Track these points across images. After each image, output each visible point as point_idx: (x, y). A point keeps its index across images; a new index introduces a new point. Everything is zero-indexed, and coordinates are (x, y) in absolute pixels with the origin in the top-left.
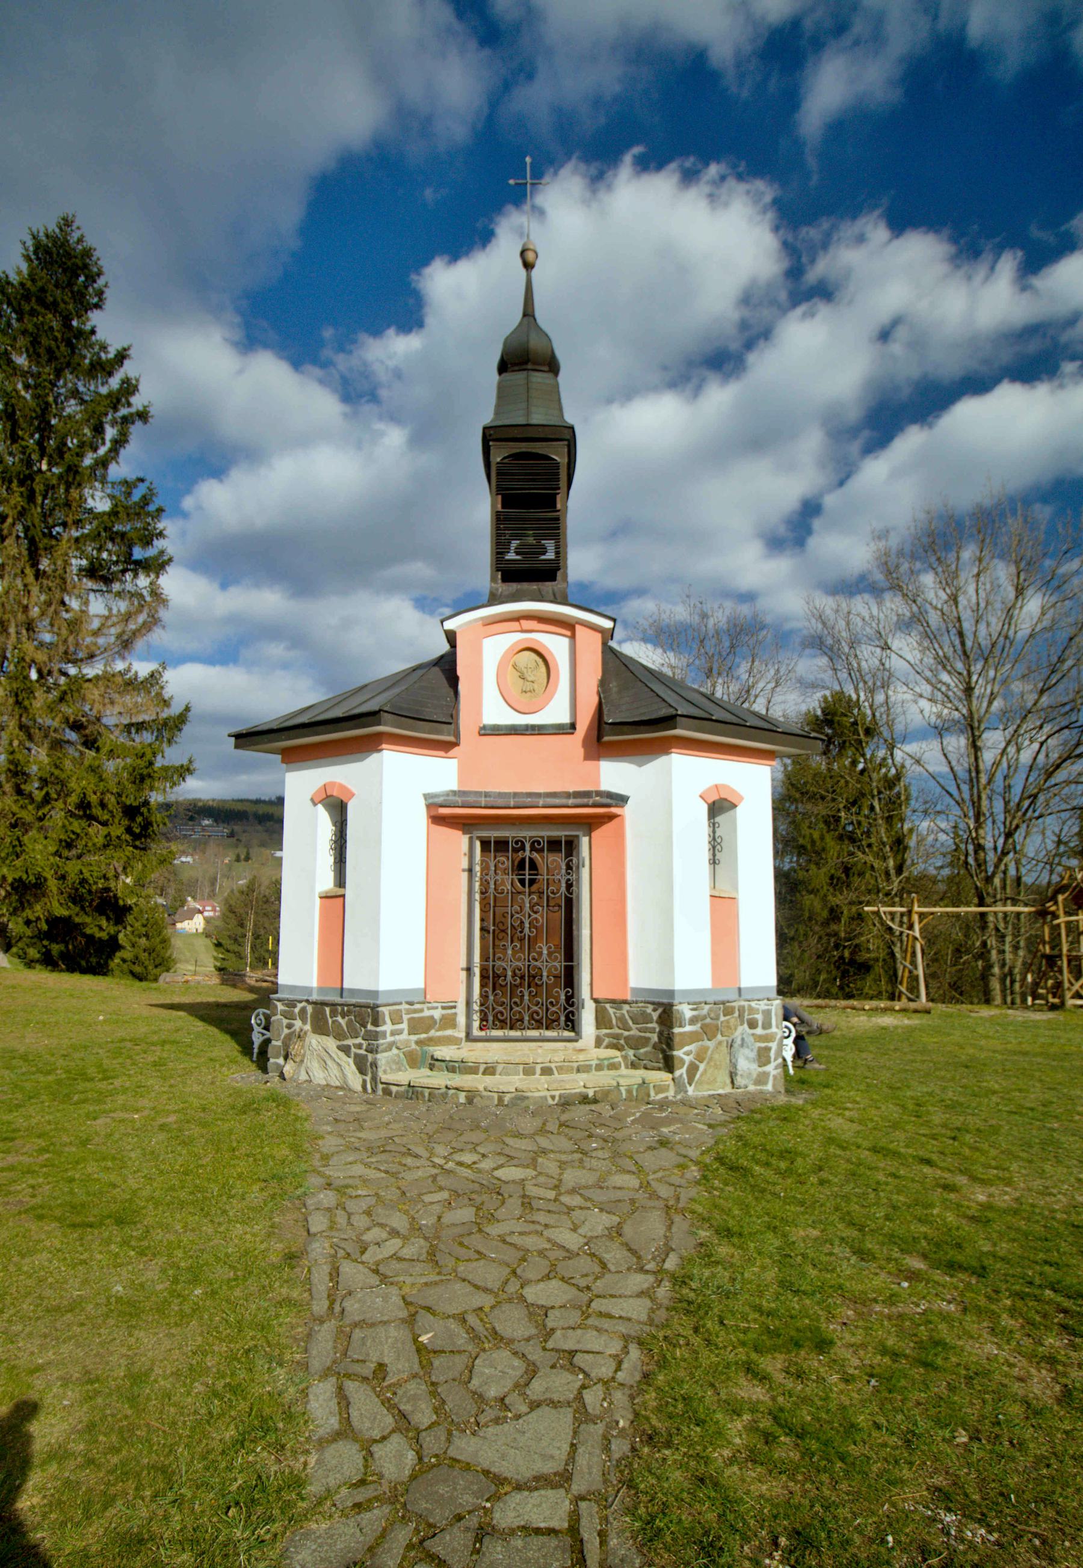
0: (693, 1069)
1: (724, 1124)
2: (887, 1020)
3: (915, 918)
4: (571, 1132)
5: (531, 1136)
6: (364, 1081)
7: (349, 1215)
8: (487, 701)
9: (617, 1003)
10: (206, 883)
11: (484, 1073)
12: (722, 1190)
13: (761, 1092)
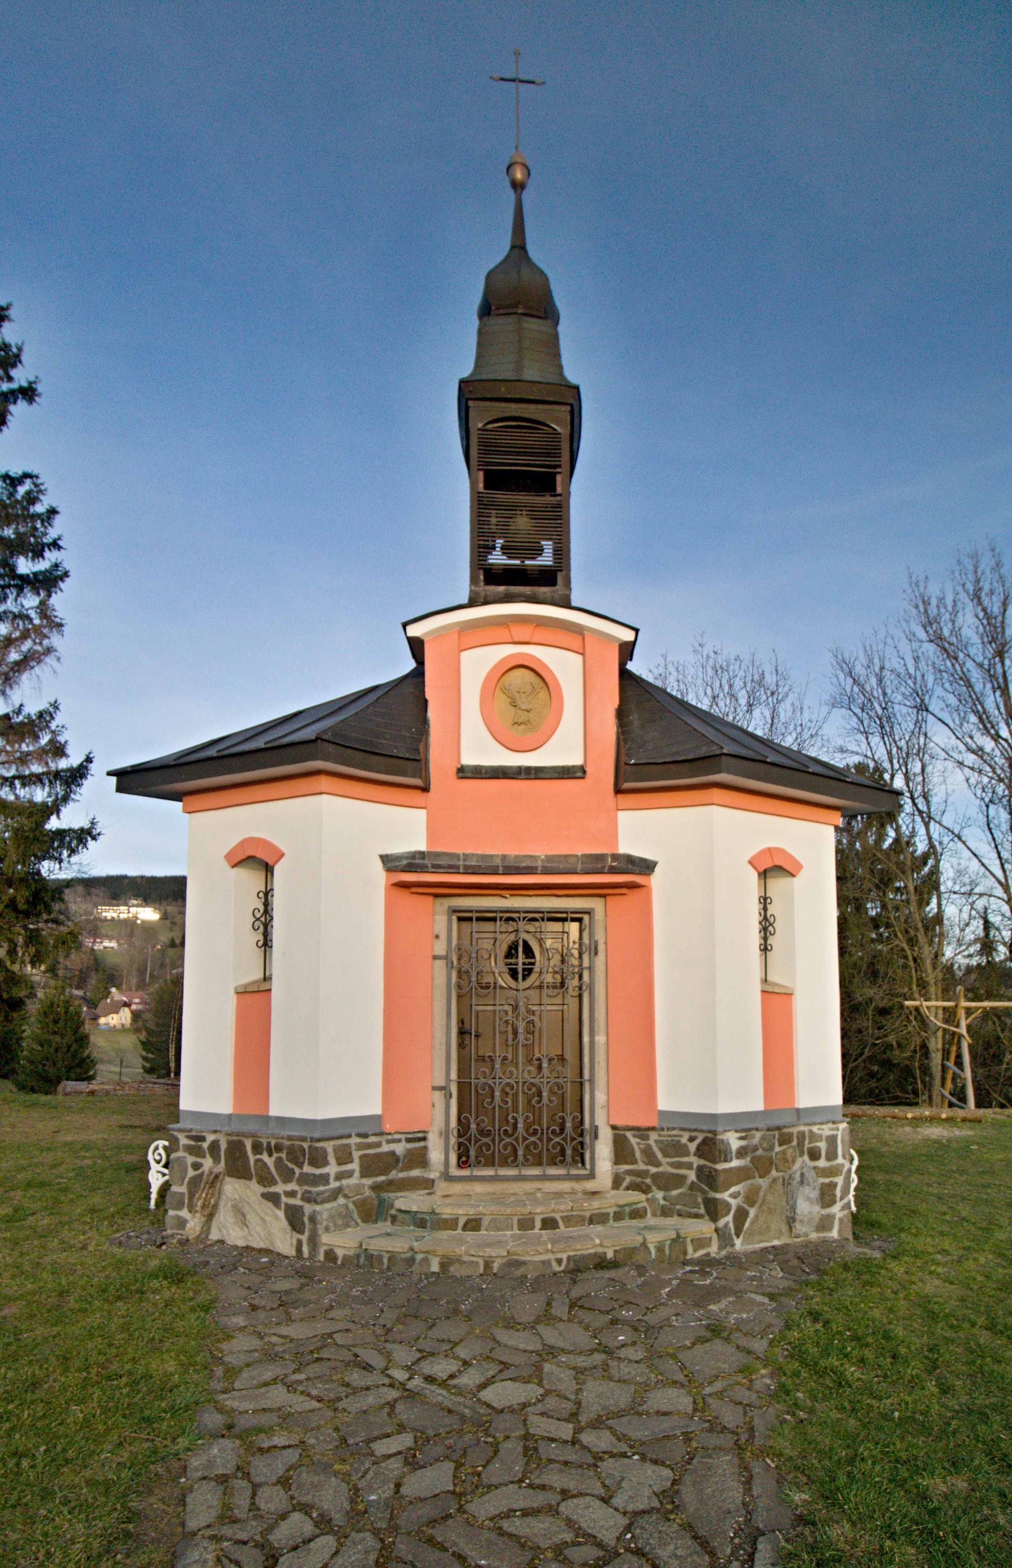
0: (741, 1215)
1: (788, 1292)
2: (935, 1132)
3: (962, 1014)
4: (587, 1317)
5: (532, 1326)
6: (300, 1243)
7: (255, 1487)
8: (468, 734)
9: (643, 1132)
10: (135, 973)
11: (465, 1228)
12: (812, 1411)
13: (825, 1241)
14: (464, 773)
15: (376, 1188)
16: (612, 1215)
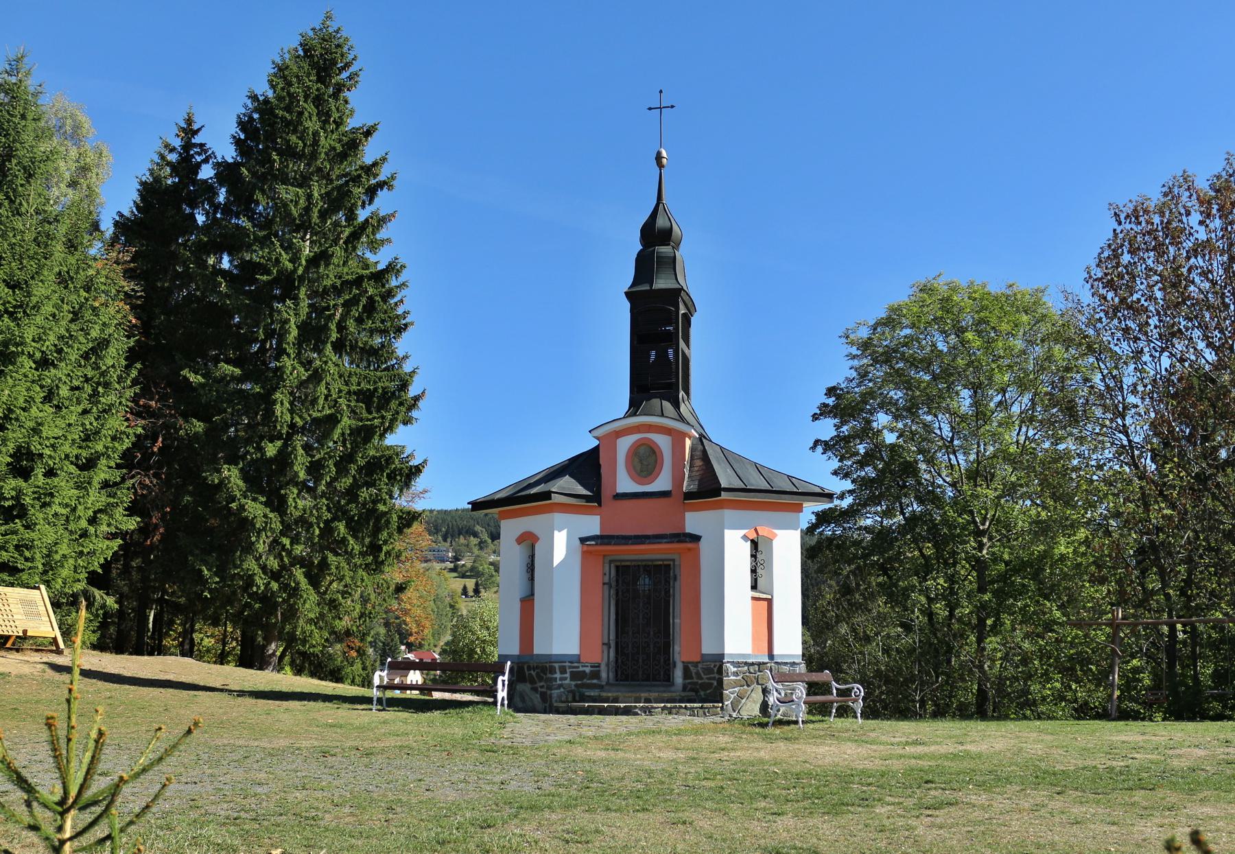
9: (696, 664)
15: (576, 686)
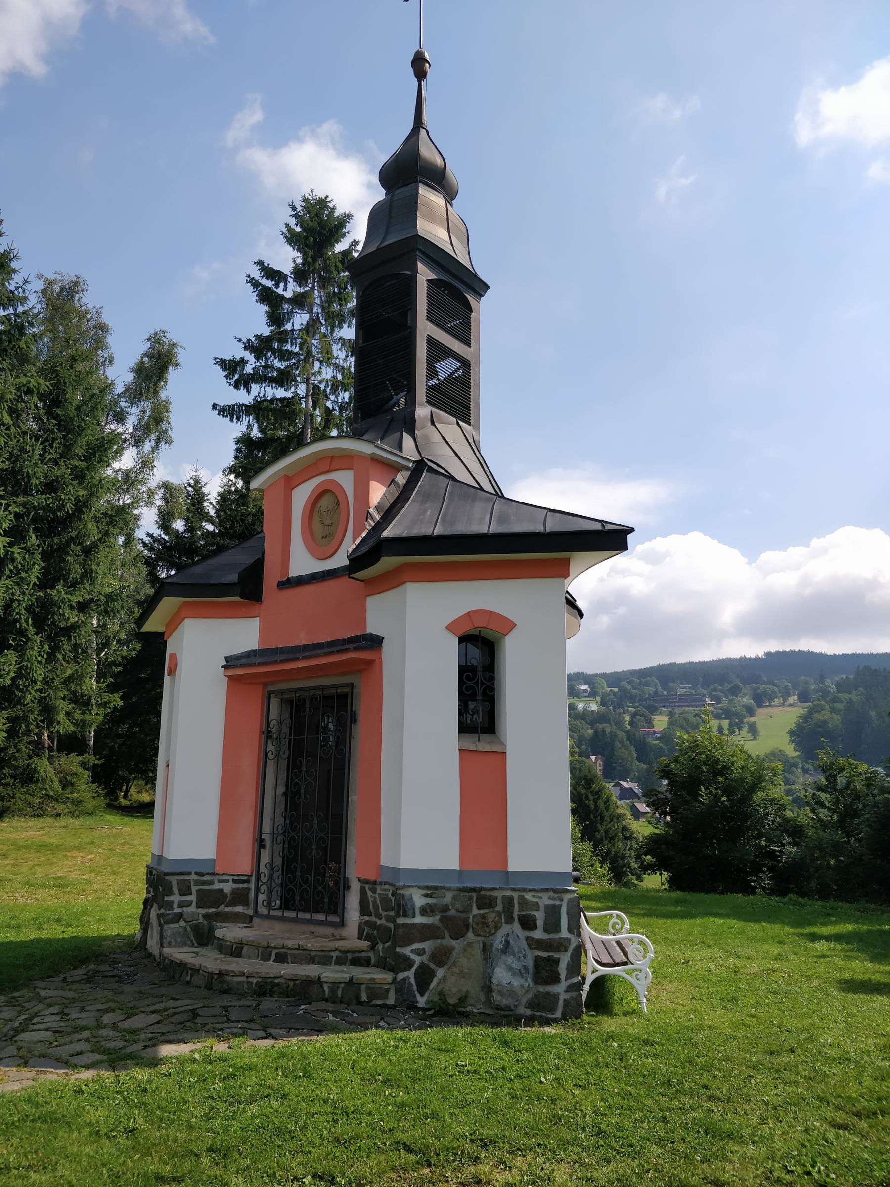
14: (288, 583)
15: (206, 916)
16: (334, 958)
